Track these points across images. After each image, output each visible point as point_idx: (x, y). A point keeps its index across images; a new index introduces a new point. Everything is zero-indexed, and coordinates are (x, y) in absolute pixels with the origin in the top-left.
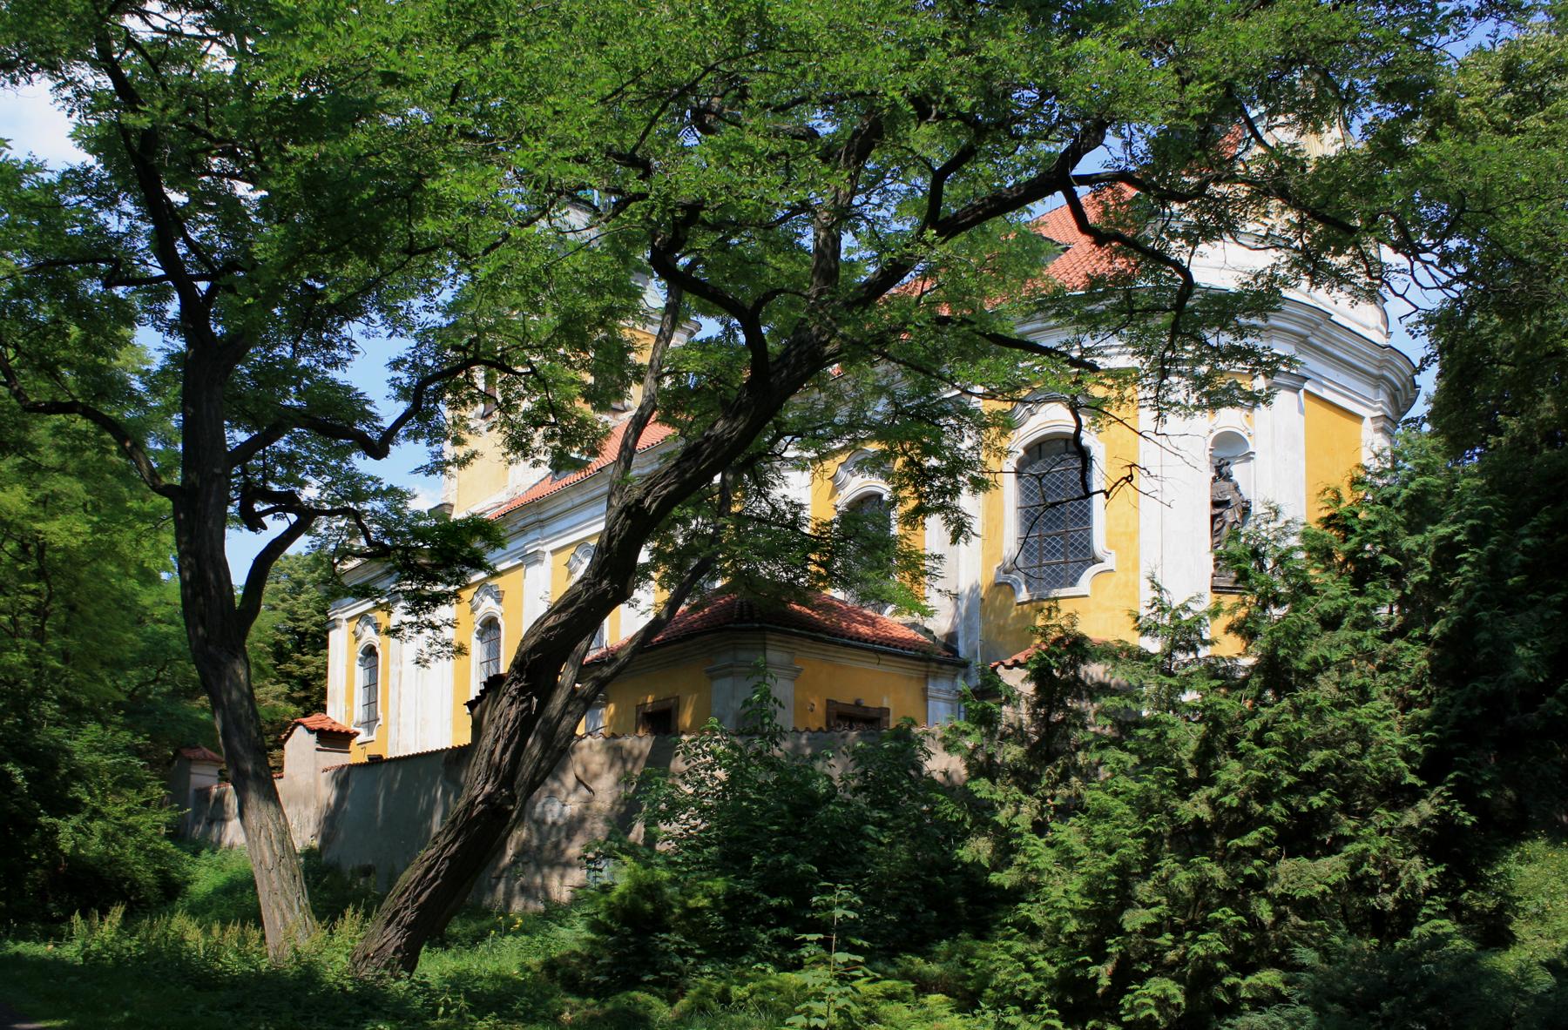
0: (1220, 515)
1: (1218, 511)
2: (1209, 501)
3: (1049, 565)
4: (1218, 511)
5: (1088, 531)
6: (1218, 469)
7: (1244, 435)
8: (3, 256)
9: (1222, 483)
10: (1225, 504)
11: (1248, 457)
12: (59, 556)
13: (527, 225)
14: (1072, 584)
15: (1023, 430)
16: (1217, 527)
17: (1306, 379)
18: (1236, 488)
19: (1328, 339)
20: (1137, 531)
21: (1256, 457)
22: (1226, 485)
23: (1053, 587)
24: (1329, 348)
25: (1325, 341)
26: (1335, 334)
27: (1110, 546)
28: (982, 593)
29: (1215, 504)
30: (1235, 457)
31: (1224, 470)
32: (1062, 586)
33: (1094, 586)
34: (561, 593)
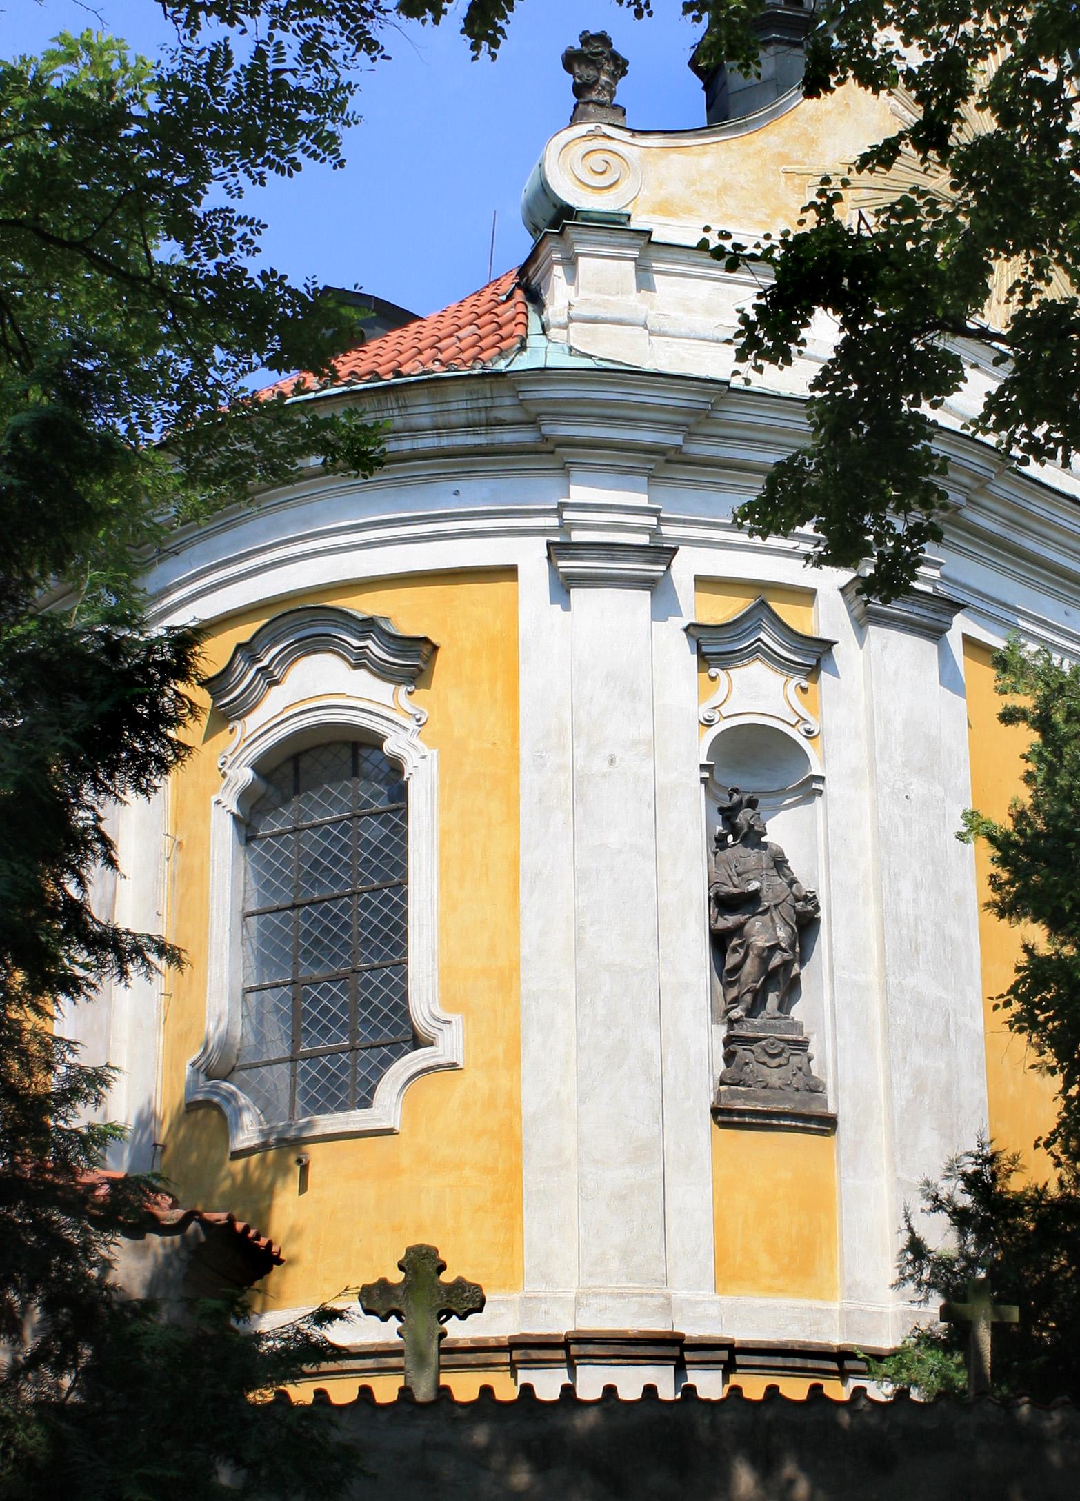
0: (738, 930)
1: (730, 921)
2: (700, 894)
3: (313, 1057)
4: (730, 921)
5: (401, 966)
6: (728, 814)
7: (796, 735)
8: (2, 274)
9: (738, 852)
10: (746, 902)
11: (810, 789)
12: (160, 1362)
13: (764, 222)
14: (366, 1103)
15: (254, 721)
16: (731, 960)
17: (958, 607)
18: (779, 863)
19: (1021, 519)
20: (515, 968)
21: (829, 787)
22: (751, 856)
23: (322, 1110)
24: (1029, 544)
25: (1012, 523)
26: (1038, 507)
27: (449, 1002)
28: (162, 1134)
29: (723, 903)
30: (782, 792)
31: (743, 817)
32: (342, 1107)
33: (410, 1110)
34: (594, 1329)
